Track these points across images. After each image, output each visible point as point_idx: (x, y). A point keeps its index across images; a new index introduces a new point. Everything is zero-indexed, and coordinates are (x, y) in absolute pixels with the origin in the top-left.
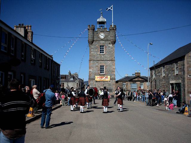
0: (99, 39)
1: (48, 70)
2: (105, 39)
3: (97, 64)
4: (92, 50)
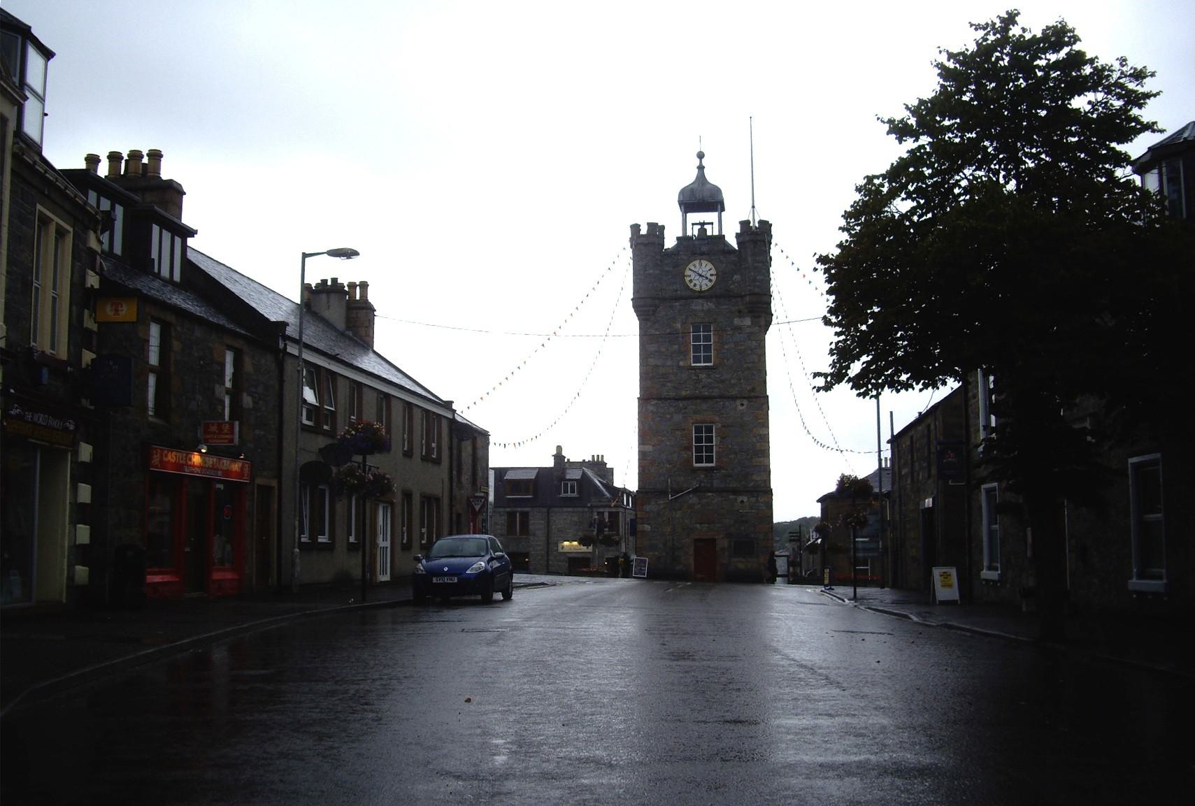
1: (438, 462)
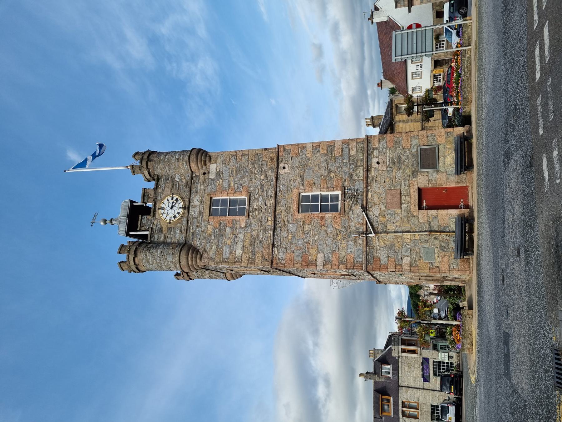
0: (185, 223)
2: (185, 194)
3: (292, 228)
4: (226, 252)
